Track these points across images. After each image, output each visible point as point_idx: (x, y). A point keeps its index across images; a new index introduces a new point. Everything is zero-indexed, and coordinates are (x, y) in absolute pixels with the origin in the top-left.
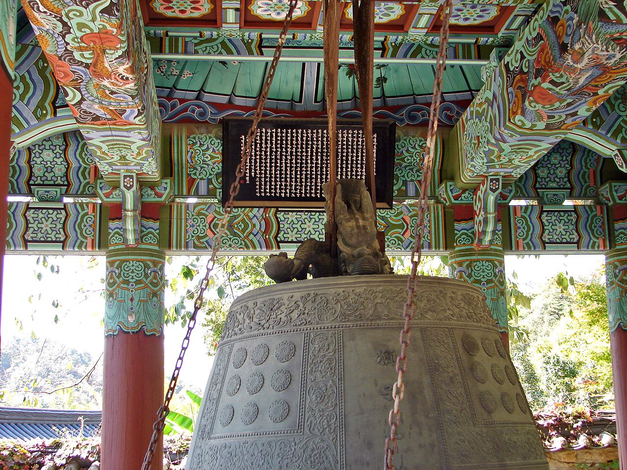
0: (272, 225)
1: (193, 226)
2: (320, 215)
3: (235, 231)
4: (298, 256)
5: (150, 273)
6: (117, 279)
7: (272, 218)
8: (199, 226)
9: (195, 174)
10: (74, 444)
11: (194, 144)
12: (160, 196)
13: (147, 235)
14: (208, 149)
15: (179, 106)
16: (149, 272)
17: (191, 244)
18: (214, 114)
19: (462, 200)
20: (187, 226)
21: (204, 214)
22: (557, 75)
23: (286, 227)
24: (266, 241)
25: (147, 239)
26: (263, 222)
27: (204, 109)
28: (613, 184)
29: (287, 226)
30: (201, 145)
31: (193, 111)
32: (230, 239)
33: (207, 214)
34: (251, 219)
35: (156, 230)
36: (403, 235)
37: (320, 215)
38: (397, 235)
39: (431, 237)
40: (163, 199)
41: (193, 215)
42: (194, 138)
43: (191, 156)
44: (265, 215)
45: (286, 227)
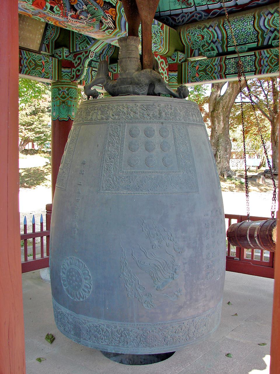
0: (223, 68)
1: (190, 72)
2: (229, 60)
3: (207, 72)
4: (181, 83)
5: (61, 93)
6: (67, 96)
7: (223, 64)
8: (193, 72)
9: (193, 47)
10: (277, 182)
11: (189, 33)
12: (174, 60)
13: (171, 79)
14: (195, 34)
15: (190, 15)
16: (60, 92)
17: (190, 81)
18: (206, 16)
19: (68, 58)
20: (188, 73)
21: (46, 73)
22: (58, 9)
23: (229, 67)
24: (220, 76)
25: (171, 81)
26: (262, 63)
27: (201, 15)
28: (65, 49)
29: (230, 66)
30: (192, 33)
31: (196, 16)
32: (205, 76)
33: (196, 66)
34: (268, 65)
35: (176, 76)
36: (199, 67)
37: (229, 60)
38: (202, 67)
39: (187, 68)
40: (175, 61)
41: (190, 68)
42: (189, 30)
43: (189, 39)
44: (220, 63)
45: (229, 67)
